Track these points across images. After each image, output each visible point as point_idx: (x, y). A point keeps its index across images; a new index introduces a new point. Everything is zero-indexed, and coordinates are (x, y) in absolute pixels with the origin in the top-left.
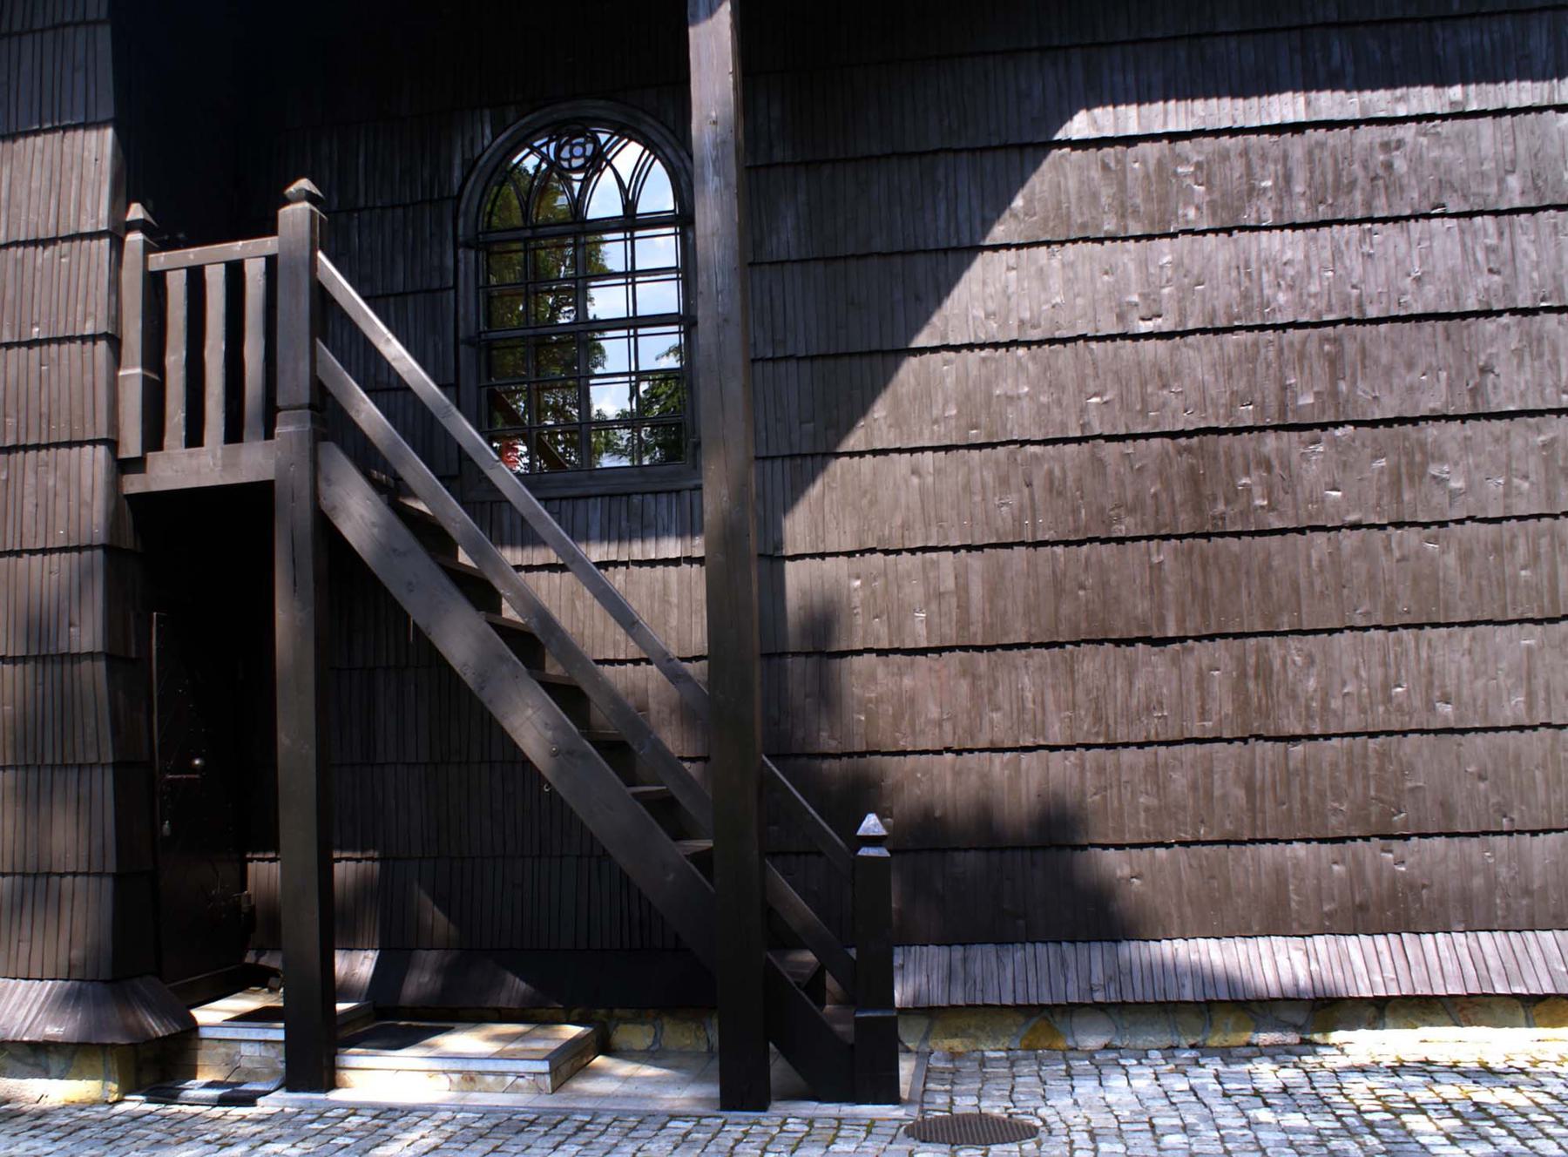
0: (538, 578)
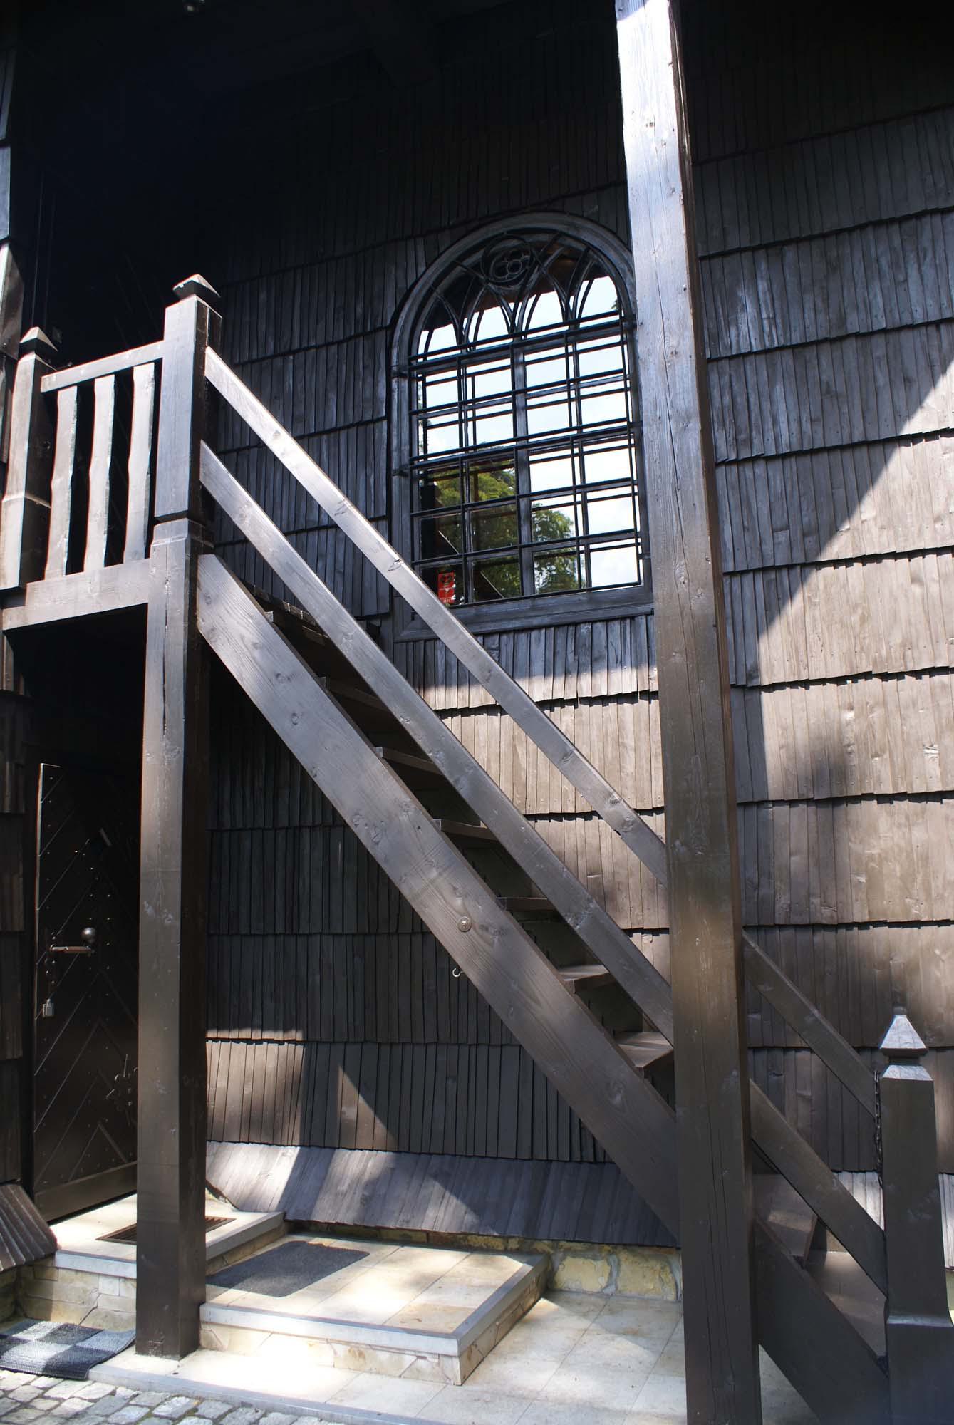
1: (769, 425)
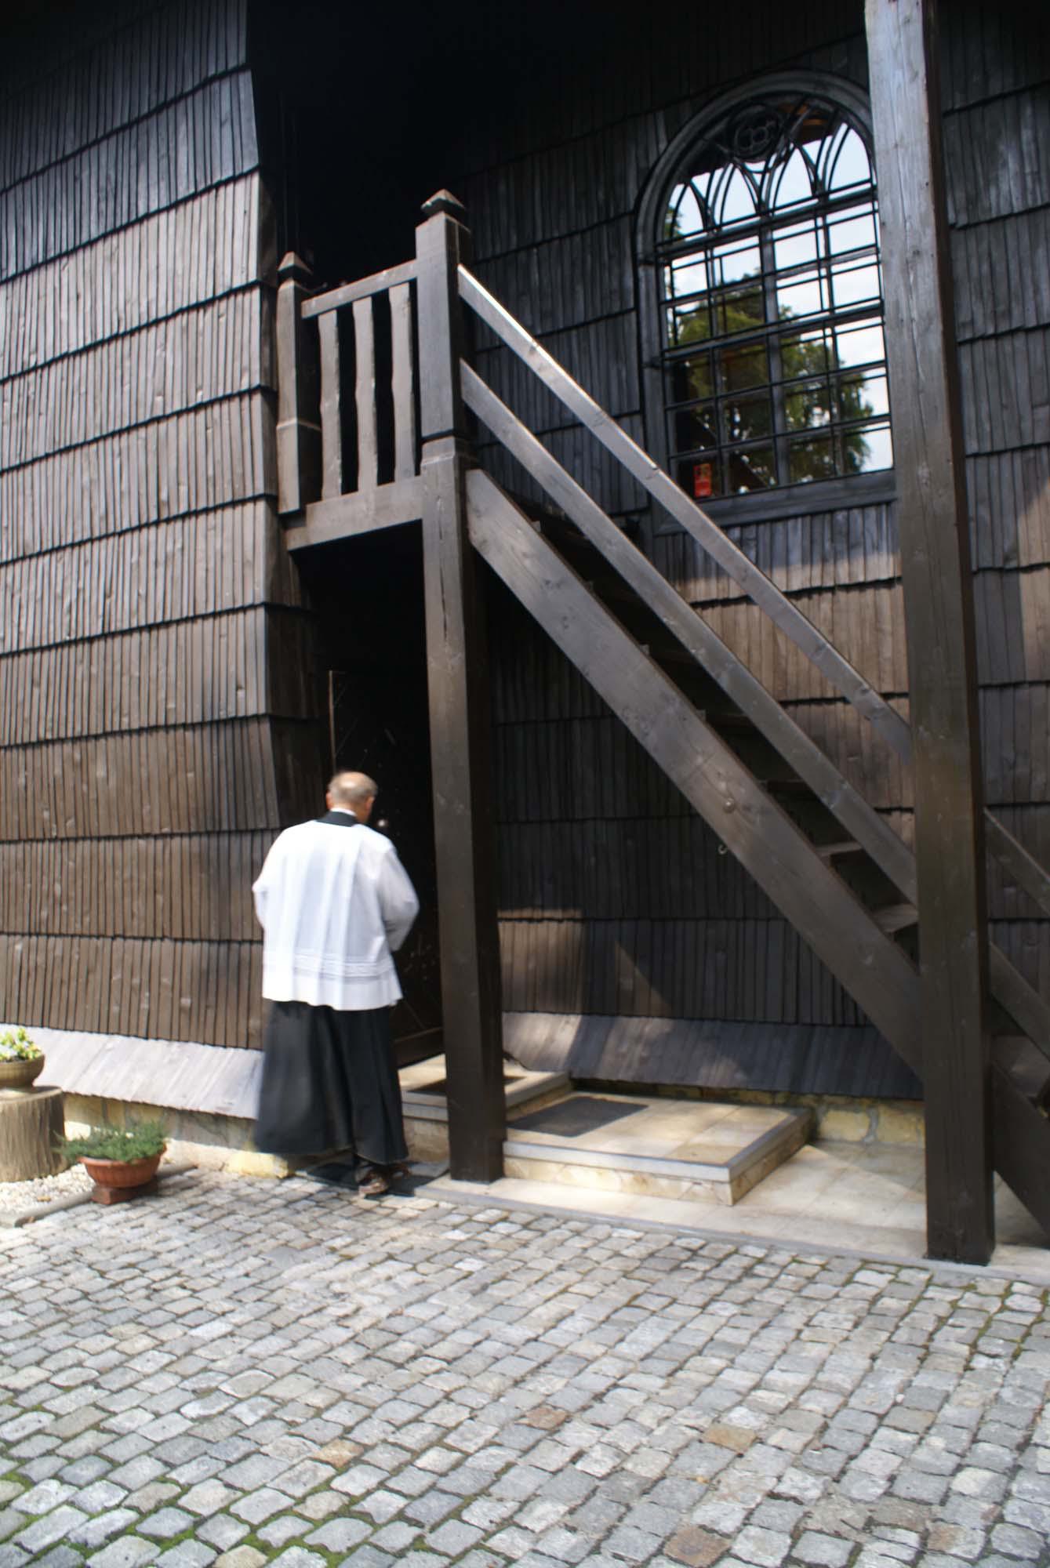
0: (736, 612)
1: (1030, 293)
